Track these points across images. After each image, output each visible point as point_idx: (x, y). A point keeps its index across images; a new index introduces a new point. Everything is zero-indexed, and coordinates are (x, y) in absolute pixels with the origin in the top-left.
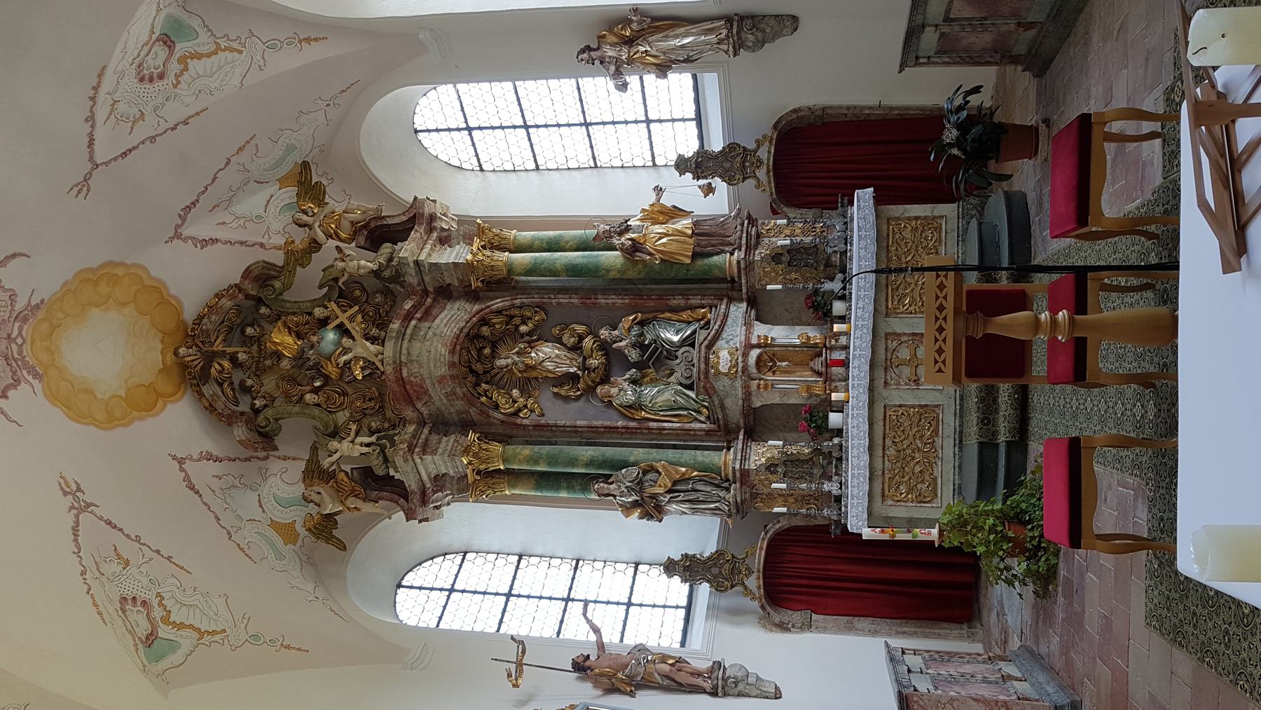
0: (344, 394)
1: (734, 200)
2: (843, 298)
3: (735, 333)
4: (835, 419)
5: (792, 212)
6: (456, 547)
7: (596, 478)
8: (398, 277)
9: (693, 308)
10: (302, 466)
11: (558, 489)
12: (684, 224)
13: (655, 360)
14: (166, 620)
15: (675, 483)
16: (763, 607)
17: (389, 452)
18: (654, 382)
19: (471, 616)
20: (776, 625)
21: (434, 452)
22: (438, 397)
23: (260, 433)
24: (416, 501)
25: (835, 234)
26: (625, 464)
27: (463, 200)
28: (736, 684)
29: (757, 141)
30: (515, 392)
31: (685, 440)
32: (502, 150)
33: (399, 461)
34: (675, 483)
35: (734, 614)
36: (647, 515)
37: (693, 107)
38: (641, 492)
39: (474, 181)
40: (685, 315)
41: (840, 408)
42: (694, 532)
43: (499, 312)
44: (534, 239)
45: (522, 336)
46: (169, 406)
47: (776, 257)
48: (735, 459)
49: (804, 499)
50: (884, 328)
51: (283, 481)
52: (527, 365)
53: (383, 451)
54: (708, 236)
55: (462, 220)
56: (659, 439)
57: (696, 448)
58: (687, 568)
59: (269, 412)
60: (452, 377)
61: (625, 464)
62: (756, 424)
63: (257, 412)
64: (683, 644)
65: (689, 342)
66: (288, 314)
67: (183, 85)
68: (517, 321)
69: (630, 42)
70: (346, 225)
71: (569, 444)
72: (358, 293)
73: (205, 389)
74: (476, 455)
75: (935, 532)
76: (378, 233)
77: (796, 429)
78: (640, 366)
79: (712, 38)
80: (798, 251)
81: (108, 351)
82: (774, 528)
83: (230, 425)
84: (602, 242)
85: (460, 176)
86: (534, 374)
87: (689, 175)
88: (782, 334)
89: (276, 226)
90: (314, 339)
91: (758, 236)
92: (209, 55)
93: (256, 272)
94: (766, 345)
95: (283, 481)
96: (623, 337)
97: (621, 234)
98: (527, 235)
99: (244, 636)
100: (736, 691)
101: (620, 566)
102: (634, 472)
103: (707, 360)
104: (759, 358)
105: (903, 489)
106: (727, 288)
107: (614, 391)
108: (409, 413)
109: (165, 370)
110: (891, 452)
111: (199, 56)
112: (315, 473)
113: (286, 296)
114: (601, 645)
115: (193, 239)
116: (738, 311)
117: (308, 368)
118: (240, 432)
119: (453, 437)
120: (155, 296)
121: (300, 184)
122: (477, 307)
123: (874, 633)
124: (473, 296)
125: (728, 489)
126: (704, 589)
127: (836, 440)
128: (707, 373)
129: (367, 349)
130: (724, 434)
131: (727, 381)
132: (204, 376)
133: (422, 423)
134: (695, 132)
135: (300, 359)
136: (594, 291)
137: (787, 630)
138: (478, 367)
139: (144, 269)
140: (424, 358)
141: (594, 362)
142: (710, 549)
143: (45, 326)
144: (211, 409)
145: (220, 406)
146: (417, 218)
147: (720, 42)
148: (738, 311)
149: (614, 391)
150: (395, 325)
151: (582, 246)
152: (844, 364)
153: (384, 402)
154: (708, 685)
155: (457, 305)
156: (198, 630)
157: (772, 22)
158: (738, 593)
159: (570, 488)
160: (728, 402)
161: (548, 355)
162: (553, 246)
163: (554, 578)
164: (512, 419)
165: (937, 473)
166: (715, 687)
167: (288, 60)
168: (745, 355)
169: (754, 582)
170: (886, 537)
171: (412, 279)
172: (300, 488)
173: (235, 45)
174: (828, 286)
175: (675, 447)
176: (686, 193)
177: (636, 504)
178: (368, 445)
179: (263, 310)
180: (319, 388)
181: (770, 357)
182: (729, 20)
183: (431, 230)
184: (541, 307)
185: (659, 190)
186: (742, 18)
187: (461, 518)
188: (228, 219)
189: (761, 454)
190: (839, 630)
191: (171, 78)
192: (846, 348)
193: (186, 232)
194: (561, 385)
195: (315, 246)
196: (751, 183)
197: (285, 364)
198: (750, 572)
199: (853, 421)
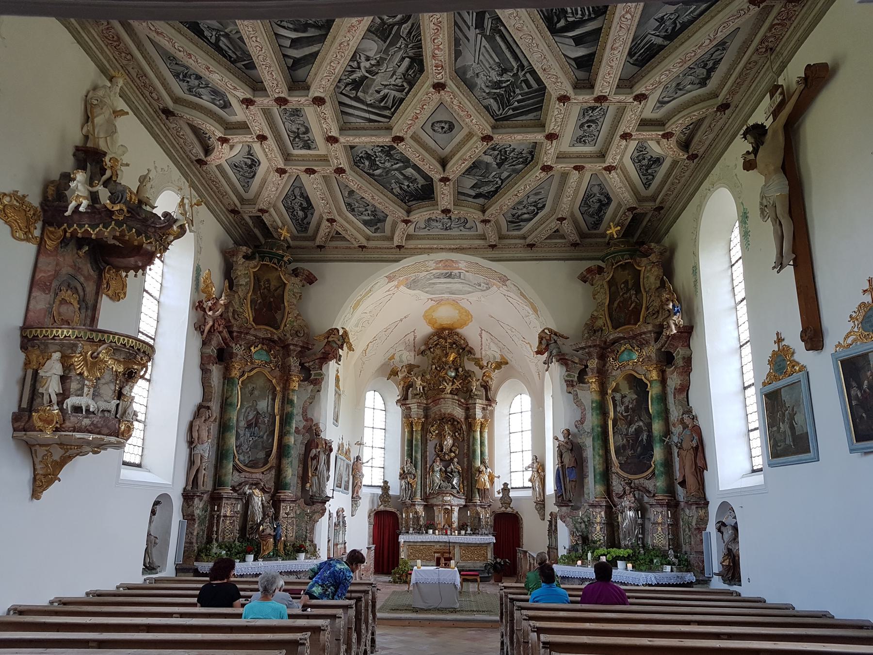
4: (431, 531)
5: (492, 518)
8: (471, 397)
13: (447, 477)
18: (441, 475)
19: (368, 413)
22: (435, 409)
24: (403, 401)
27: (499, 410)
31: (424, 486)
39: (506, 412)
41: (434, 533)
47: (478, 514)
49: (407, 522)
51: (409, 357)
54: (484, 493)
55: (492, 413)
58: (385, 487)
65: (453, 487)
76: (486, 387)
78: (446, 472)
81: (446, 315)
82: (398, 513)
88: (455, 515)
96: (455, 466)
98: (486, 435)
106: (469, 499)
112: (410, 368)
113: (466, 357)
116: (462, 502)
117: (442, 367)
118: (423, 348)
120: (463, 324)
124: (467, 417)
130: (426, 498)
135: (446, 363)
146: (490, 401)
148: (462, 502)
150: (456, 397)
152: (446, 534)
153: (433, 393)
159: (408, 450)
161: (449, 442)
162: (482, 444)
169: (382, 508)
171: (470, 402)
181: (449, 512)
182: (544, 501)
185: (499, 477)
189: (420, 509)
195: (482, 368)
197: (444, 359)
199: (431, 536)
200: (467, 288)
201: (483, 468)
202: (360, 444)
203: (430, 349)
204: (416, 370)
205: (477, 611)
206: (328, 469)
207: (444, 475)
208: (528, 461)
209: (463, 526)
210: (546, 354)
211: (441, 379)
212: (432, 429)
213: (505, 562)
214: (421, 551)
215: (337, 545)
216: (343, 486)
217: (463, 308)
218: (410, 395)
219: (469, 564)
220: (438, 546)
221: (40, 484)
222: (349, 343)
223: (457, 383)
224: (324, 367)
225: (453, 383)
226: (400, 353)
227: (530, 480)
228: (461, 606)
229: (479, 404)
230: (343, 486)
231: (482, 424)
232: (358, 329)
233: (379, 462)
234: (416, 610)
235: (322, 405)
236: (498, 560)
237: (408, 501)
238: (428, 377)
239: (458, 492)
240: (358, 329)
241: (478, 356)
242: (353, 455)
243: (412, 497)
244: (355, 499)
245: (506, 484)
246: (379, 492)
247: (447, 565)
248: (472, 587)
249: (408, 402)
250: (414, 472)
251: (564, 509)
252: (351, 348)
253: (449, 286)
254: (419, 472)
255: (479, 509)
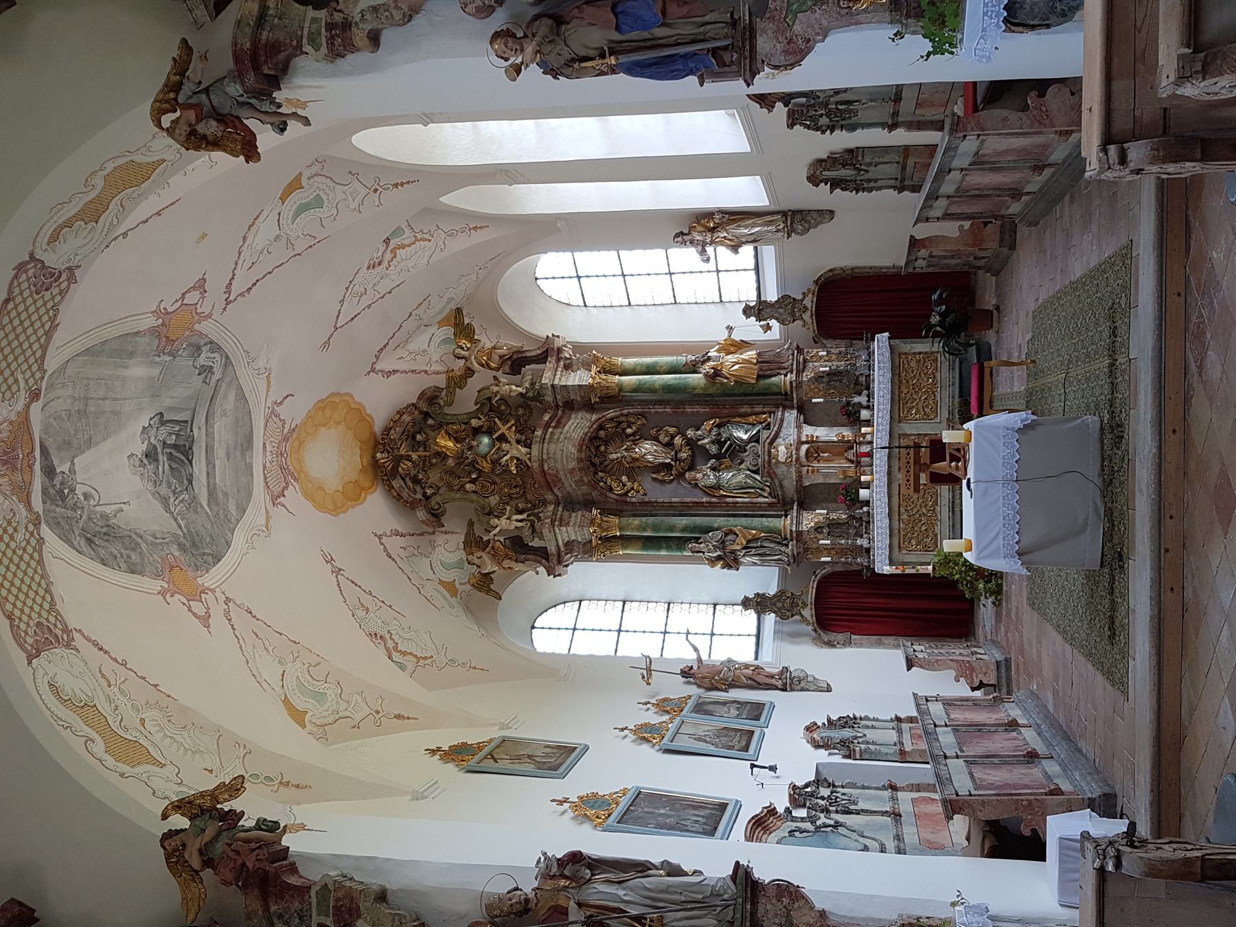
0: (495, 483)
1: (786, 336)
2: (868, 407)
3: (789, 433)
4: (864, 493)
5: (829, 343)
6: (573, 597)
7: (689, 540)
8: (538, 397)
9: (757, 414)
10: (462, 538)
11: (659, 549)
12: (750, 354)
13: (731, 453)
14: (396, 649)
15: (749, 542)
16: (815, 630)
17: (537, 525)
18: (728, 468)
19: (586, 645)
20: (825, 643)
21: (567, 524)
22: (570, 484)
23: (433, 515)
24: (552, 561)
25: (860, 363)
26: (712, 529)
27: (573, 330)
28: (800, 681)
29: (803, 293)
30: (624, 478)
31: (753, 510)
32: (598, 293)
33: (546, 532)
34: (749, 542)
35: (794, 636)
36: (727, 566)
37: (753, 261)
38: (724, 548)
39: (580, 314)
40: (750, 419)
41: (867, 486)
42: (762, 578)
43: (612, 419)
44: (637, 364)
45: (628, 436)
46: (369, 497)
47: (819, 378)
48: (792, 523)
49: (843, 551)
50: (898, 431)
51: (448, 549)
52: (633, 459)
53: (532, 526)
54: (768, 364)
55: (578, 347)
56: (734, 510)
57: (762, 516)
58: (758, 604)
59: (438, 498)
60: (580, 469)
61: (712, 529)
62: (806, 498)
63: (427, 498)
64: (756, 659)
65: (755, 439)
66: (448, 424)
67: (392, 267)
68: (624, 425)
69: (712, 230)
70: (496, 357)
71: (666, 515)
72: (503, 407)
73: (394, 483)
74: (600, 526)
75: (930, 568)
76: (516, 363)
77: (835, 501)
78: (718, 457)
79: (773, 228)
80: (835, 374)
81: (332, 458)
82: (821, 573)
83: (413, 509)
84: (693, 368)
85: (568, 310)
86: (637, 464)
87: (753, 319)
88: (824, 433)
89: (436, 357)
90: (475, 443)
91: (805, 361)
92: (409, 246)
93: (429, 394)
94: (813, 442)
95: (448, 549)
96: (705, 436)
97: (704, 362)
98: (630, 361)
99: (445, 661)
100: (799, 687)
101: (702, 607)
102: (719, 534)
103: (770, 452)
104: (808, 450)
105: (913, 542)
106: (783, 400)
107: (699, 476)
108: (549, 497)
109: (363, 470)
110: (904, 517)
111: (403, 247)
112: (474, 543)
113: (447, 410)
114: (700, 660)
115: (382, 371)
116: (791, 416)
117: (467, 466)
118: (421, 514)
119: (580, 513)
120: (359, 414)
121: (456, 325)
122: (594, 417)
123: (897, 647)
124: (590, 407)
125: (787, 546)
126: (770, 619)
127: (865, 509)
128: (770, 462)
129: (519, 450)
130: (782, 506)
131: (784, 468)
132: (394, 472)
133: (558, 504)
134: (754, 278)
135: (460, 457)
136: (681, 403)
137: (834, 646)
138: (597, 461)
139: (351, 396)
140: (558, 456)
141: (684, 455)
142: (772, 590)
143: (297, 443)
144: (399, 497)
145: (405, 495)
146: (548, 352)
147: (778, 231)
148: (791, 416)
149: (699, 476)
150: (539, 433)
151: (673, 370)
152: (870, 455)
153: (530, 489)
154: (779, 684)
155: (580, 415)
156: (416, 656)
157: (815, 215)
158: (796, 621)
159: (669, 548)
160: (786, 483)
161: (648, 450)
162: (651, 370)
163: (652, 616)
164: (623, 498)
165: (937, 530)
166: (785, 684)
167: (461, 243)
168: (798, 449)
169: (808, 613)
170: (899, 572)
171: (549, 398)
172: (462, 554)
173: (427, 236)
174: (857, 399)
175: (745, 516)
176: (751, 330)
177: (719, 558)
178: (521, 521)
179: (430, 422)
180: (476, 479)
181: (816, 449)
182: (784, 214)
183: (559, 360)
184: (643, 415)
185: (730, 329)
186: (794, 212)
187: (580, 573)
188: (405, 354)
189: (810, 520)
190: (871, 646)
191: (385, 263)
192: (871, 443)
193: (378, 367)
194: (658, 472)
195: (469, 372)
196: (799, 323)
197: (451, 462)
198: (805, 605)
199: (876, 494)
200: (228, 402)
201: (707, 368)
202: (648, 669)
203: (427, 498)
204: (478, 530)
205: (1112, 351)
206: (642, 868)
207: (727, 461)
208: (685, 256)
209: (849, 414)
210: (252, 124)
211: (498, 470)
212: (618, 490)
213: (940, 302)
214: (913, 527)
215: (902, 753)
216: (746, 725)
217: (309, 417)
218: (536, 543)
219: (946, 397)
220: (900, 476)
221: (912, 236)
222: (214, 795)
223: (503, 429)
224: (312, 874)
225: (503, 438)
226: (438, 568)
227: (735, 248)
228: (1096, 410)
229: (552, 376)
230: (746, 725)
231: (606, 372)
232: (331, 692)
233: (699, 618)
234: (1115, 558)
235: (429, 881)
236: (935, 319)
237: (791, 548)
238: (493, 500)
239: (768, 427)
240: (331, 692)
241: (441, 381)
242: (678, 689)
243: (780, 538)
244: (788, 682)
245: (748, 311)
246: (770, 619)
247: (959, 454)
248: (1010, 382)
249: (552, 549)
250: (719, 534)
251: (764, 44)
252: (235, 788)
253: (219, 452)
254: (720, 521)
255: (807, 375)
